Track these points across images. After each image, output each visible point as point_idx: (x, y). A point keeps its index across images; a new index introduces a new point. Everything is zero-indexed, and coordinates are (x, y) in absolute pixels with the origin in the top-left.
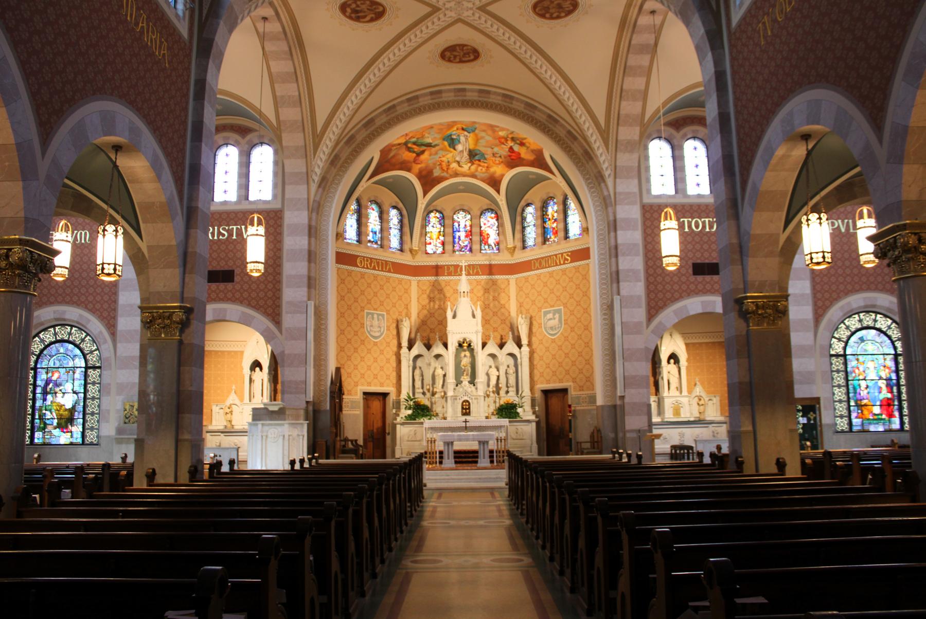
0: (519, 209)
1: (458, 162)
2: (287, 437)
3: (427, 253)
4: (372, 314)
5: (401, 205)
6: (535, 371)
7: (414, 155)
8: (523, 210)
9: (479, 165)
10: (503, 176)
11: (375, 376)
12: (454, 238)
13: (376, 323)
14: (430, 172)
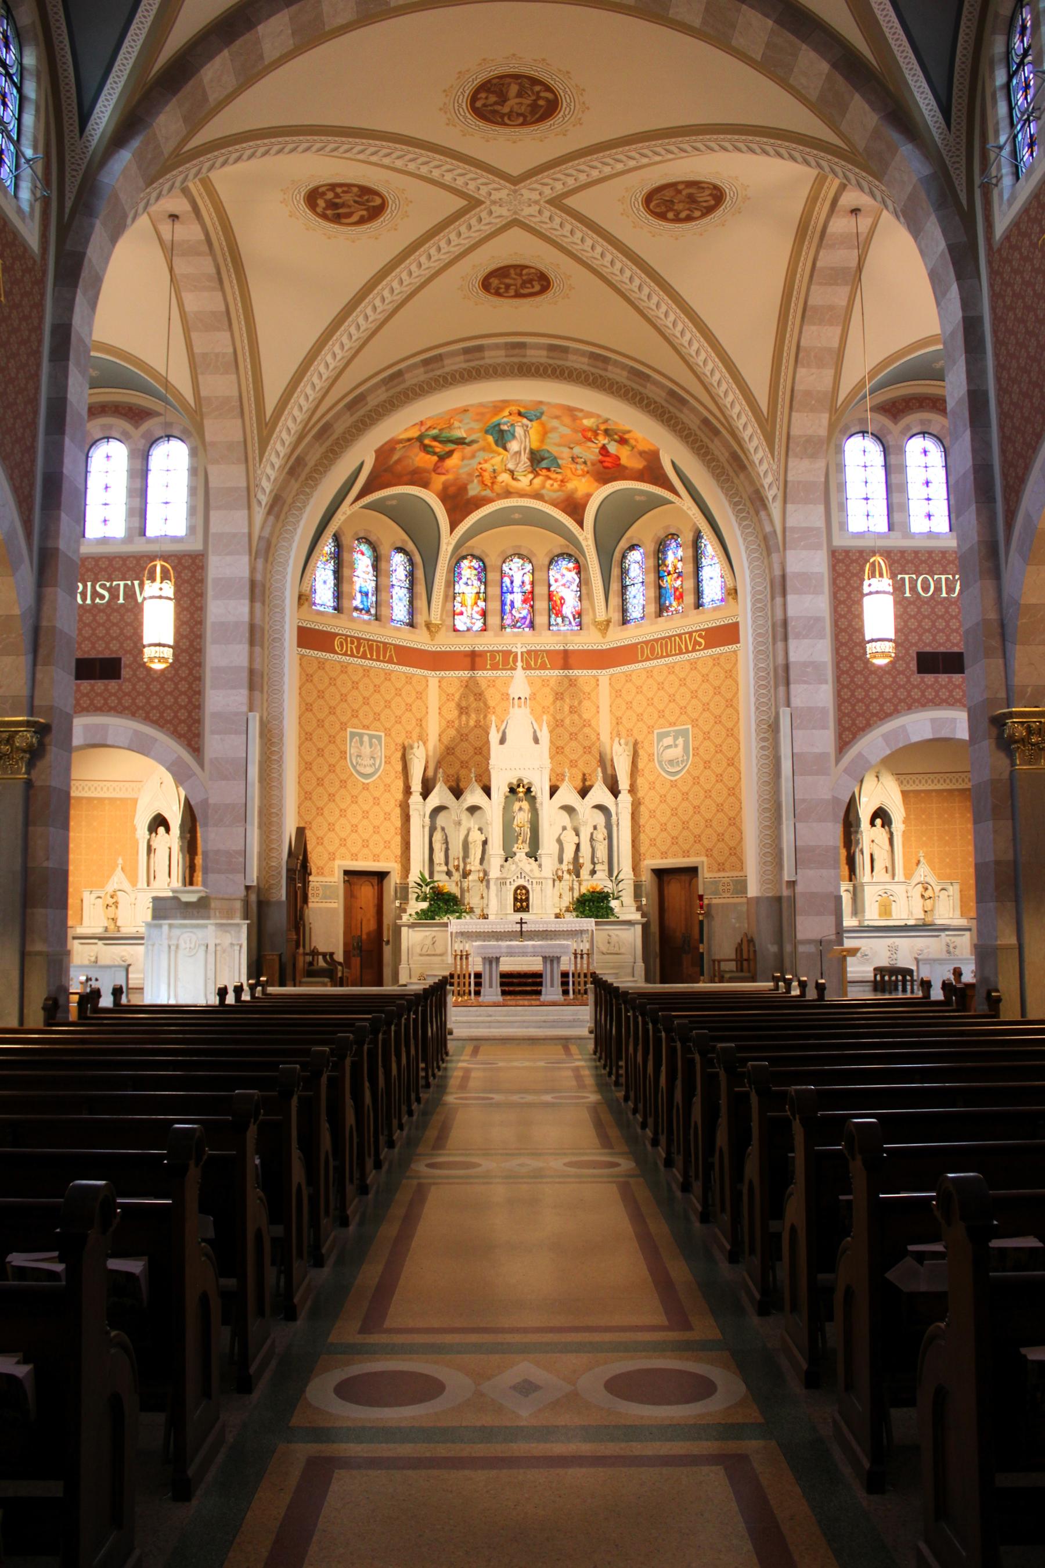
0: (617, 555)
1: (512, 472)
2: (211, 948)
4: (361, 736)
5: (410, 546)
6: (642, 836)
7: (435, 458)
8: (624, 557)
9: (549, 478)
10: (589, 496)
11: (365, 844)
12: (503, 604)
13: (366, 750)
14: (463, 488)
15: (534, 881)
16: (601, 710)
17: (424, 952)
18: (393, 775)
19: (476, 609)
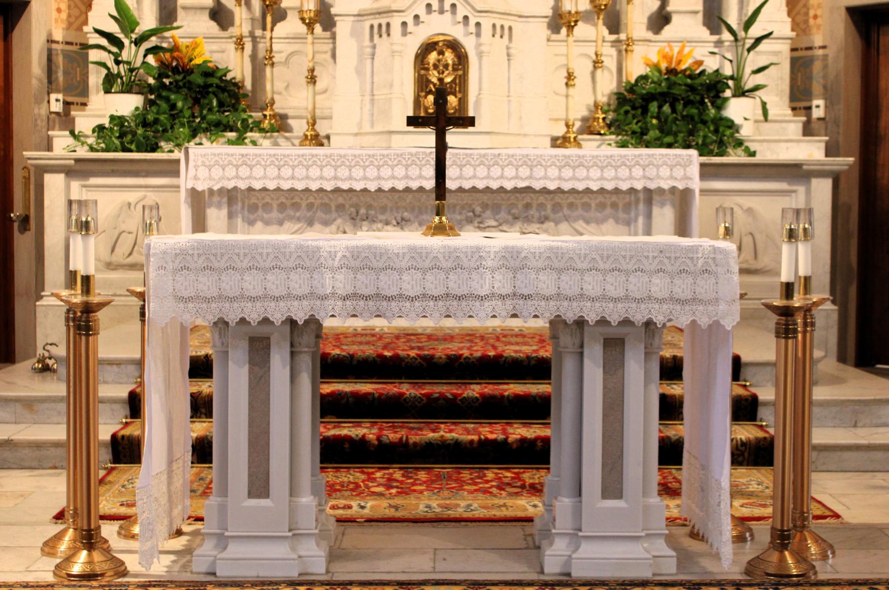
17: (120, 256)
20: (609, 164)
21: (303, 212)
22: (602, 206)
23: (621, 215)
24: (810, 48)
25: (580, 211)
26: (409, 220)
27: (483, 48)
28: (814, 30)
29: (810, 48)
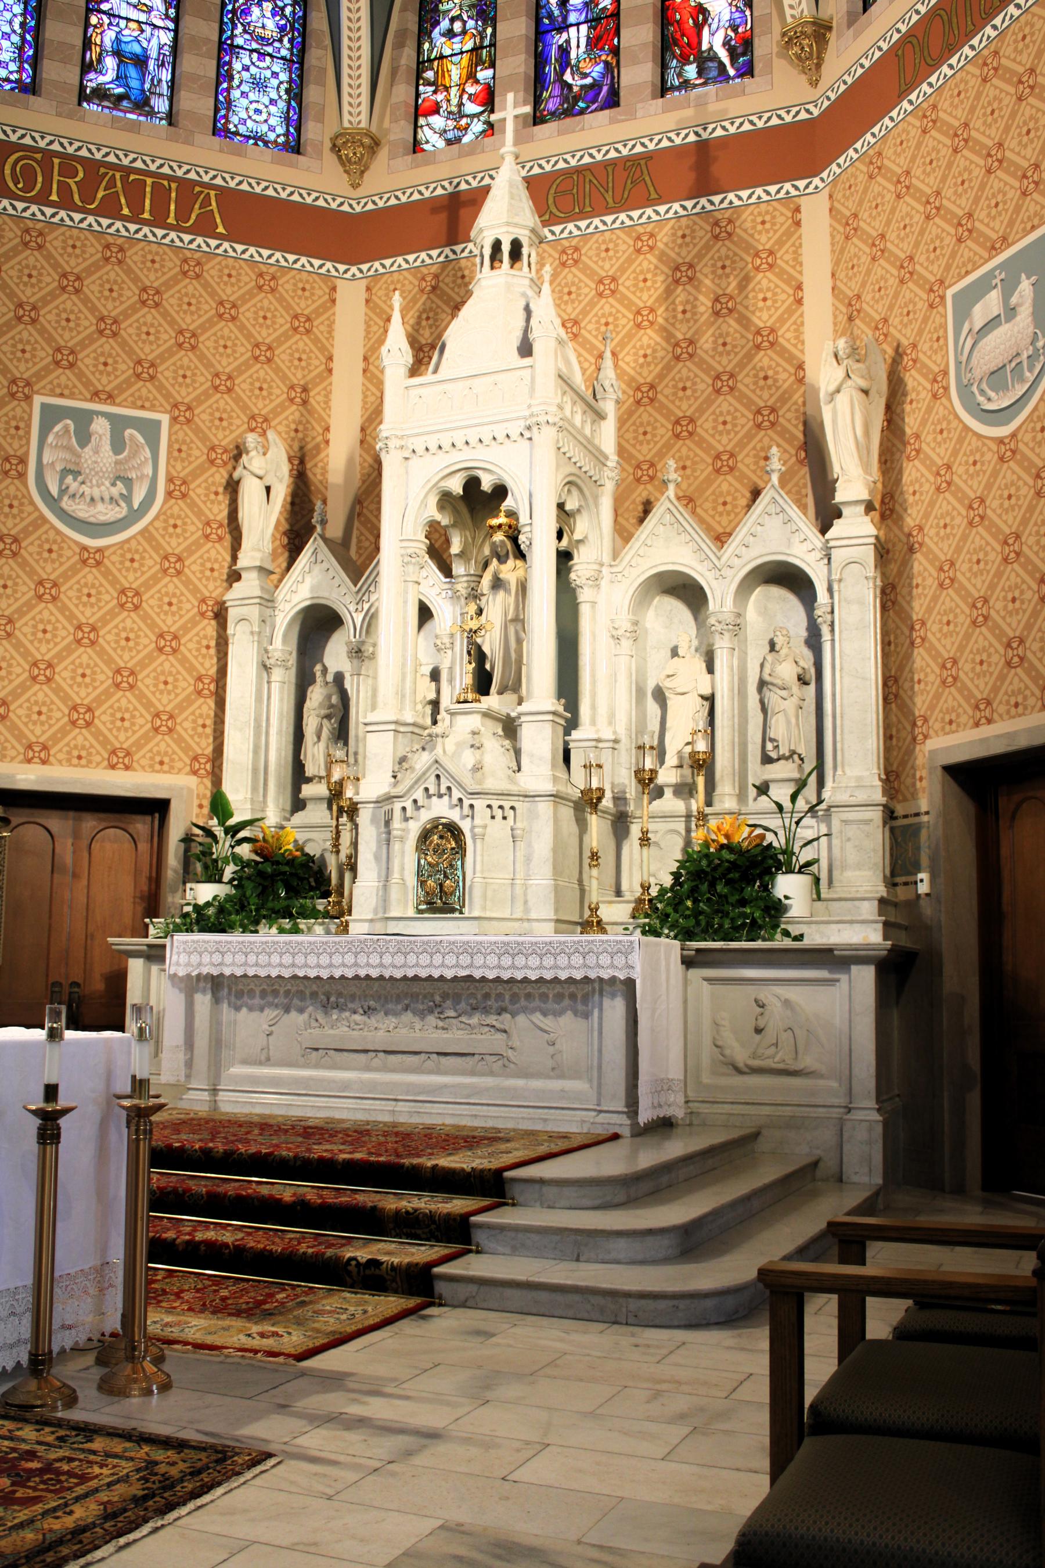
3: (416, 146)
4: (83, 419)
6: (920, 658)
11: (81, 716)
13: (100, 455)
15: (480, 804)
16: (808, 295)
18: (194, 529)
19: (471, 89)
20: (548, 952)
21: (281, 1000)
22: (559, 997)
23: (580, 1007)
24: (917, 815)
25: (537, 1003)
26: (375, 1009)
27: (476, 830)
28: (920, 795)
29: (917, 815)
